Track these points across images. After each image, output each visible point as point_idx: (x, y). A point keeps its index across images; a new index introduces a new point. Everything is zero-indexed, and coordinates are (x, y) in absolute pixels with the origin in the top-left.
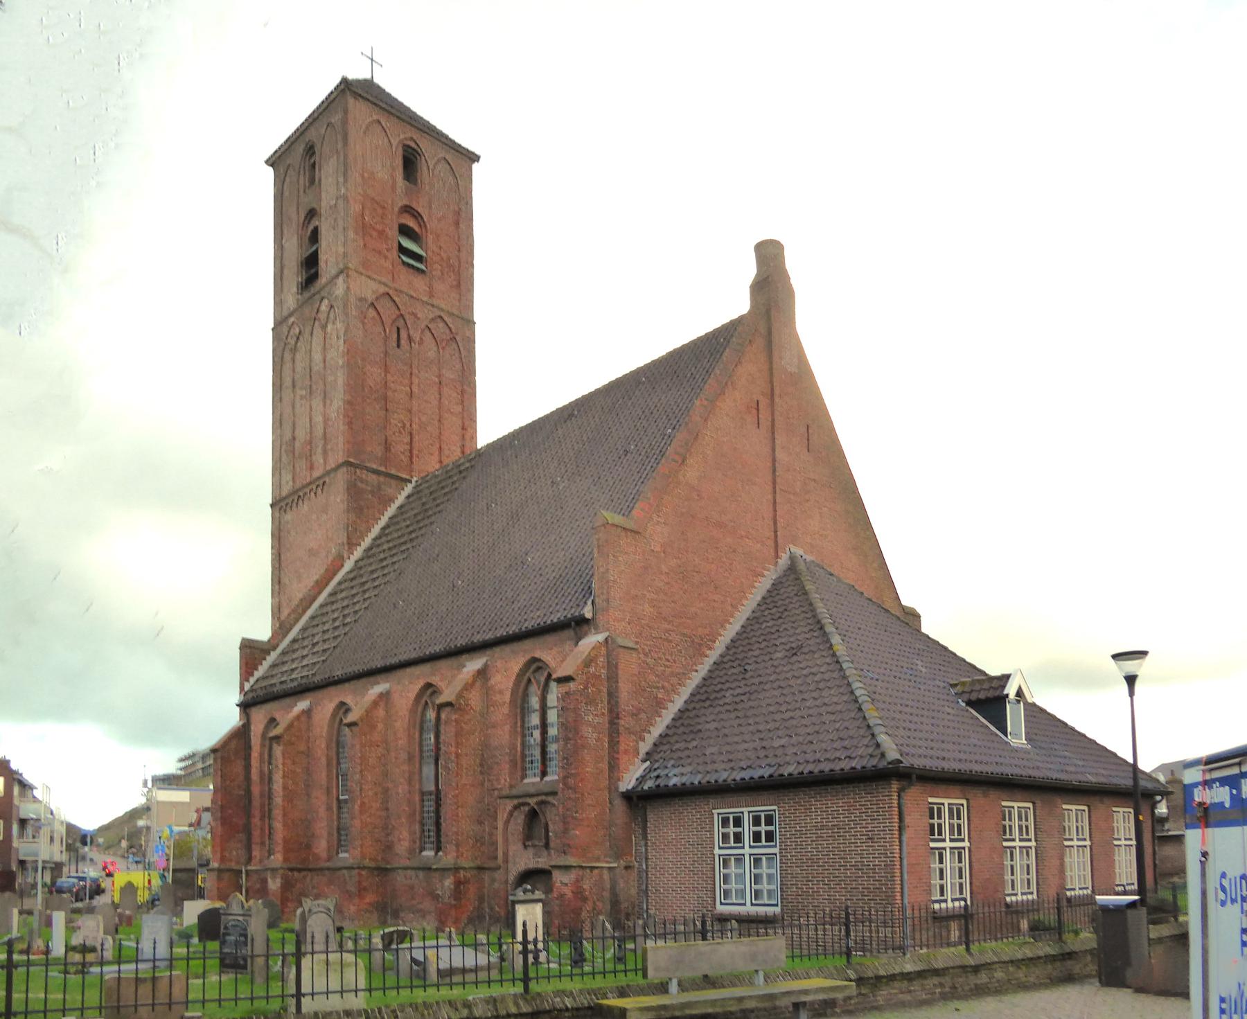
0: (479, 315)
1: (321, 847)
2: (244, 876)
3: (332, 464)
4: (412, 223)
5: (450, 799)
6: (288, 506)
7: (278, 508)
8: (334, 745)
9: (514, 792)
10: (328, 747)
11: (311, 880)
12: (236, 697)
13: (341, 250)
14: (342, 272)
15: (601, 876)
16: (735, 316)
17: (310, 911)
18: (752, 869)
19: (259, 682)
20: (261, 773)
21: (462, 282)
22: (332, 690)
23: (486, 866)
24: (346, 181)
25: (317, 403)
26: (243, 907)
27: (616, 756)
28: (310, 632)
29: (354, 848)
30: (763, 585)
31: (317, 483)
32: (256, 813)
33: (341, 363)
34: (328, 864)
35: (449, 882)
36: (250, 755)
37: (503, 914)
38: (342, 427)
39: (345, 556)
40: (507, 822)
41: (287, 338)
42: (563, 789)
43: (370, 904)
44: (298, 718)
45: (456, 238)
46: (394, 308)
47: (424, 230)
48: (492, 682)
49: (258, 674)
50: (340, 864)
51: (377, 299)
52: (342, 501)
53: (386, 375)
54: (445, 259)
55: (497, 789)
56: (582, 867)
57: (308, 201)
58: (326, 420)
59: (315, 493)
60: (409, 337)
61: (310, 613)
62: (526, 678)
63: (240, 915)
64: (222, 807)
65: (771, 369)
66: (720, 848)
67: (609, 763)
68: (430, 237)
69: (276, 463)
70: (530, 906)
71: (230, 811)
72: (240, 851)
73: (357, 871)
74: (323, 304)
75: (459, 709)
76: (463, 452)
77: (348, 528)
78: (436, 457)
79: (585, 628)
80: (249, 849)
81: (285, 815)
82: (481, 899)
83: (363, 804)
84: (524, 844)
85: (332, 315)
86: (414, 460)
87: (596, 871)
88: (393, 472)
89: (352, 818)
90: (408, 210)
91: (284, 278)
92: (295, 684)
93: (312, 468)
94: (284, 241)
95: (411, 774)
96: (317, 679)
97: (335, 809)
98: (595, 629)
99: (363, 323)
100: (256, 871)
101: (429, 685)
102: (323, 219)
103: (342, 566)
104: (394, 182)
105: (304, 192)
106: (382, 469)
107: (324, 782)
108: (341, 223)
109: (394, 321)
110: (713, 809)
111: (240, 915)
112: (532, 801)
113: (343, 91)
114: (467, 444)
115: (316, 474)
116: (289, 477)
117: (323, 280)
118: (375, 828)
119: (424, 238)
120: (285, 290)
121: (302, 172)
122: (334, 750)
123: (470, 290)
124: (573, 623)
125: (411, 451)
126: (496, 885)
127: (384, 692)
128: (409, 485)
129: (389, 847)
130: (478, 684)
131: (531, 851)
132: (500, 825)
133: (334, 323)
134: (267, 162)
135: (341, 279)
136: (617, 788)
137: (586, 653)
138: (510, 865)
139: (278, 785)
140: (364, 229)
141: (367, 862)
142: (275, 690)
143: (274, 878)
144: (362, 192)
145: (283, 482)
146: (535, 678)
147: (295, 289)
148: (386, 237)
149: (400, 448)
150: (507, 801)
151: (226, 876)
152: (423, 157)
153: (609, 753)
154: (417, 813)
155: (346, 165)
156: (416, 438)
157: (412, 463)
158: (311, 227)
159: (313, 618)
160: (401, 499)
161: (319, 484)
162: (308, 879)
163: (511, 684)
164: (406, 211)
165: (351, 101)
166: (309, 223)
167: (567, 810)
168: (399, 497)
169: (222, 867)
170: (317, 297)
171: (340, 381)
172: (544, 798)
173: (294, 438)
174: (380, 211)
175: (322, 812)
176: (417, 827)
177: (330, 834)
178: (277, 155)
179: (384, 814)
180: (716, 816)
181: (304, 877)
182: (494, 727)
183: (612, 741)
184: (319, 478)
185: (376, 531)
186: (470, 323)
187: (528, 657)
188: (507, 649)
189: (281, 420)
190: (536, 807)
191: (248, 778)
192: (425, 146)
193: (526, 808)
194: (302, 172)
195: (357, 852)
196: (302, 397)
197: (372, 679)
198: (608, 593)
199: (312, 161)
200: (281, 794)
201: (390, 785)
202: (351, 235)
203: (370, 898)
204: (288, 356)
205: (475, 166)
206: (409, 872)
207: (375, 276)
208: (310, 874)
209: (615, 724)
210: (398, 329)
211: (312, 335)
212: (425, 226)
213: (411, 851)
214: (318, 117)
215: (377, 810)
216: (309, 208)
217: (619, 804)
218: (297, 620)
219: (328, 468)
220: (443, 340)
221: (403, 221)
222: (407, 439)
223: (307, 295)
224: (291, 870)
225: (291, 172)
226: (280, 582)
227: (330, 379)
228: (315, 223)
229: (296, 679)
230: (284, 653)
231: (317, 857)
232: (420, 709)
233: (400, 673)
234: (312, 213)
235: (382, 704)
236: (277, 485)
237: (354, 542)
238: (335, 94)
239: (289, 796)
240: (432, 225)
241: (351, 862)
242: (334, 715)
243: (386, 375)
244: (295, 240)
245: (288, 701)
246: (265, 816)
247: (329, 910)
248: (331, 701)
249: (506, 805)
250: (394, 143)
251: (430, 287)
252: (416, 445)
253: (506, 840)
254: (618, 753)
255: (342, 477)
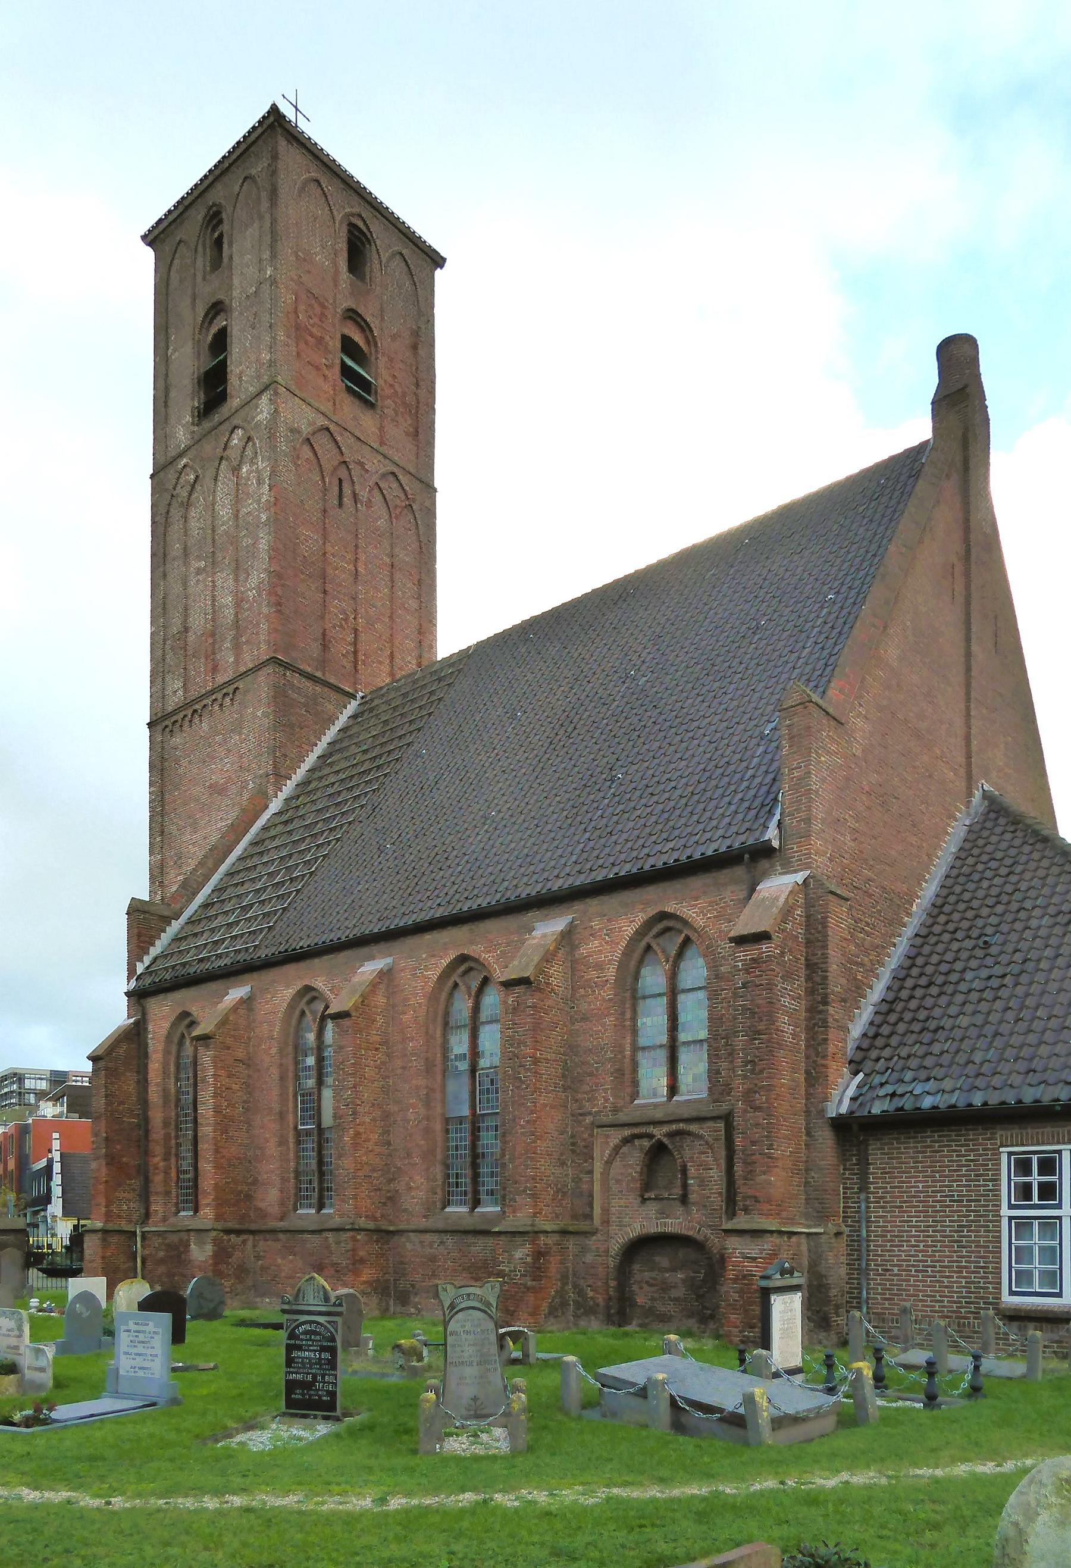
0: (441, 479)
1: (270, 1198)
2: (139, 1239)
3: (248, 661)
4: (358, 338)
5: (522, 1127)
6: (178, 725)
7: (160, 728)
8: (290, 1049)
9: (622, 1117)
10: (281, 1051)
11: (254, 1246)
12: (120, 984)
13: (265, 356)
14: (266, 388)
15: (799, 1245)
16: (915, 443)
17: (452, 1306)
18: (1013, 1241)
19: (158, 962)
20: (165, 1092)
21: (420, 431)
22: (291, 969)
23: (571, 1229)
24: (274, 256)
25: (224, 579)
26: (327, 1299)
27: (820, 1061)
28: (231, 892)
29: (343, 1201)
30: (956, 832)
31: (225, 691)
32: (158, 1150)
33: (264, 517)
34: (281, 1225)
35: (522, 1253)
36: (146, 1066)
37: (600, 1300)
38: (265, 610)
39: (271, 792)
40: (609, 1163)
41: (174, 489)
42: (745, 1111)
43: (365, 1282)
44: (235, 1009)
45: (414, 368)
46: (336, 451)
47: (373, 348)
48: (583, 951)
49: (154, 951)
50: (300, 1224)
51: (314, 434)
52: (265, 715)
53: (324, 544)
54: (400, 394)
55: (590, 1113)
56: (780, 1232)
57: (209, 292)
58: (239, 602)
59: (221, 705)
60: (355, 496)
61: (223, 868)
62: (643, 944)
63: (320, 1313)
64: (107, 1139)
65: (967, 521)
66: (1011, 1207)
67: (807, 1072)
68: (382, 361)
69: (157, 665)
70: (787, 1297)
71: (118, 1147)
72: (132, 1205)
73: (350, 1234)
74: (235, 436)
75: (539, 990)
76: (419, 665)
77: (274, 751)
78: (386, 668)
79: (764, 864)
80: (145, 1196)
81: (217, 1151)
82: (564, 1278)
83: (358, 1134)
84: (642, 1196)
85: (249, 452)
86: (359, 667)
87: (794, 1239)
88: (332, 680)
89: (340, 1157)
90: (352, 316)
91: (171, 403)
92: (227, 961)
93: (215, 669)
94: (170, 351)
95: (431, 1090)
96: (263, 953)
97: (291, 1145)
98: (782, 866)
99: (297, 466)
100: (158, 1233)
101: (463, 958)
102: (236, 314)
103: (267, 807)
104: (337, 273)
105: (204, 279)
106: (319, 674)
107: (276, 1107)
108: (265, 318)
109: (335, 469)
110: (1002, 1146)
111: (320, 1313)
112: (659, 1132)
113: (271, 126)
114: (426, 655)
115: (221, 679)
116: (178, 684)
117: (234, 402)
118: (374, 1170)
119: (373, 358)
120: (173, 420)
121: (200, 249)
122: (291, 1057)
123: (430, 443)
124: (747, 856)
125: (355, 653)
126: (589, 1258)
127: (386, 968)
128: (353, 702)
129: (392, 1199)
130: (561, 954)
131: (652, 1208)
132: (598, 1167)
133: (252, 463)
134: (144, 238)
135: (264, 399)
136: (822, 1112)
137: (782, 900)
138: (613, 1228)
139: (207, 1109)
140: (299, 331)
141: (362, 1222)
142: (192, 970)
143: (201, 1244)
144: (296, 278)
145: (169, 691)
146: (658, 945)
147: (188, 418)
148: (326, 348)
149: (341, 648)
150: (612, 1131)
151: (114, 1239)
152: (374, 247)
153: (807, 1057)
154: (439, 1150)
155: (273, 233)
156: (363, 637)
157: (356, 671)
158: (214, 330)
159: (230, 874)
160: (342, 720)
161: (229, 690)
162: (250, 1243)
163: (618, 954)
164: (350, 318)
165: (282, 143)
166: (211, 323)
167: (753, 1143)
168: (340, 716)
169: (110, 1226)
170: (227, 426)
171: (263, 545)
172: (681, 1126)
173: (186, 630)
174: (318, 310)
175: (272, 1148)
176: (438, 1171)
177: (284, 1180)
178: (161, 227)
179: (384, 1150)
180: (1004, 1158)
181: (244, 1242)
182: (584, 1019)
183: (814, 1039)
184: (229, 683)
185: (311, 759)
186: (430, 490)
187: (652, 911)
188: (611, 902)
189: (164, 603)
190: (665, 1140)
191: (144, 1102)
192: (377, 229)
193: (646, 1143)
194: (200, 249)
195: (348, 1206)
196: (199, 571)
197: (364, 951)
198: (809, 808)
199: (216, 235)
200: (212, 1120)
201: (393, 1108)
202: (281, 336)
203: (367, 1274)
204: (176, 513)
205: (438, 273)
206: (428, 1237)
207: (312, 401)
208: (251, 1237)
209: (820, 1012)
210: (340, 480)
211: (216, 480)
212: (376, 344)
213: (429, 1210)
214: (228, 169)
215: (376, 1144)
216: (213, 300)
217: (826, 1138)
218: (207, 878)
219: (243, 669)
220: (396, 506)
221: (346, 332)
222: (350, 638)
223: (207, 425)
224: (228, 1232)
225: (182, 248)
226: (162, 833)
227: (247, 541)
228: (220, 323)
229: (227, 954)
230: (190, 922)
231: (263, 1215)
232: (444, 995)
233: (411, 942)
234: (217, 308)
235: (382, 988)
236: (158, 695)
237: (283, 772)
238: (260, 131)
239: (224, 1124)
240: (384, 343)
241: (337, 1221)
242: (291, 1007)
243: (324, 544)
244: (188, 348)
245: (213, 986)
246: (170, 1154)
247: (488, 1304)
248: (288, 987)
249: (607, 1136)
250: (338, 217)
251: (381, 428)
252: (362, 647)
253: (606, 1189)
254: (824, 1057)
255: (263, 684)
